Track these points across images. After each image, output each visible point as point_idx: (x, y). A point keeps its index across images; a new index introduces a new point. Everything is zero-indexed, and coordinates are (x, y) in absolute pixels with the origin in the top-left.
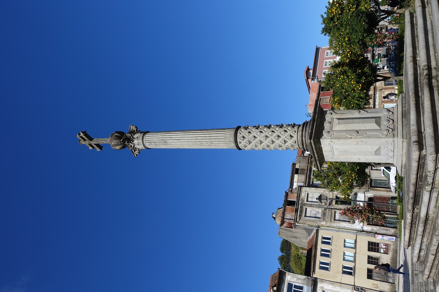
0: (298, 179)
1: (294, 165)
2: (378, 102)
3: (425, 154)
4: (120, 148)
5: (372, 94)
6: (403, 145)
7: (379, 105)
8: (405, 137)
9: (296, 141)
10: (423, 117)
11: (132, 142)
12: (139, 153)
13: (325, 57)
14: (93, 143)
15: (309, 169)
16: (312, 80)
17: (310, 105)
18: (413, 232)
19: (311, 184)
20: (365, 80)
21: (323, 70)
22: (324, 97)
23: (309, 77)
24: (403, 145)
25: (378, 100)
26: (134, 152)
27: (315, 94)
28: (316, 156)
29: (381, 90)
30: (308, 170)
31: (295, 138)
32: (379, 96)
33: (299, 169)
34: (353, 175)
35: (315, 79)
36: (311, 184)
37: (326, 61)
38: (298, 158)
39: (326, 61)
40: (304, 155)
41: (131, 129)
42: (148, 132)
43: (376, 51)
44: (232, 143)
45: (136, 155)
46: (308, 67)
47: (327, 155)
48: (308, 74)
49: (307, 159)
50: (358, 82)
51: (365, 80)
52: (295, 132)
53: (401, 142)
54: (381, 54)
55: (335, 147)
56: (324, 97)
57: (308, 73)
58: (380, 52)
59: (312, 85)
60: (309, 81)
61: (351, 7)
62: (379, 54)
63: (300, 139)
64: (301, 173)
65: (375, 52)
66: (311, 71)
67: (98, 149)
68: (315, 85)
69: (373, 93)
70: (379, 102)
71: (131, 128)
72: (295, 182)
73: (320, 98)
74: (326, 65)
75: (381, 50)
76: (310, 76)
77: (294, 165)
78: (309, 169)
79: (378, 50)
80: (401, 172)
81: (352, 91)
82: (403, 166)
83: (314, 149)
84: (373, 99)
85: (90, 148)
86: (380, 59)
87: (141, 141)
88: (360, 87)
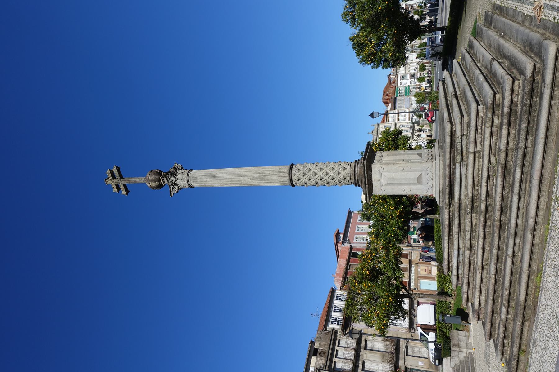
0: (316, 362)
1: (312, 343)
2: (414, 276)
3: (455, 129)
4: (156, 186)
5: (408, 268)
6: (440, 164)
7: (415, 280)
8: (442, 156)
9: (349, 173)
10: (453, 116)
11: (175, 175)
12: (177, 192)
13: (356, 231)
14: (121, 183)
15: (331, 347)
16: (342, 244)
17: (338, 275)
18: (451, 246)
19: (333, 368)
20: (402, 208)
21: (355, 235)
22: (355, 264)
23: (338, 241)
24: (440, 164)
25: (414, 274)
26: (172, 190)
27: (344, 261)
28: (367, 183)
29: (417, 264)
30: (331, 349)
31: (348, 170)
32: (415, 270)
33: (318, 349)
34: (390, 298)
35: (345, 243)
36: (333, 368)
37: (359, 226)
38: (319, 332)
39: (359, 226)
40: (326, 329)
41: (176, 167)
42: (192, 170)
43: (411, 224)
44: (286, 176)
45: (173, 193)
46: (339, 230)
47: (376, 186)
48: (337, 239)
49: (330, 334)
50: (396, 209)
51: (402, 208)
52: (348, 165)
53: (439, 160)
54: (416, 228)
55: (383, 175)
56: (355, 264)
57: (338, 237)
58: (415, 225)
59: (341, 250)
60: (338, 246)
61: (389, 148)
62: (414, 228)
63: (352, 170)
64: (320, 356)
65: (410, 224)
66: (341, 236)
67: (124, 192)
68: (346, 250)
69: (408, 266)
70: (415, 277)
71: (176, 166)
72: (312, 367)
73: (350, 264)
74: (358, 230)
75: (416, 224)
76: (340, 240)
77: (312, 343)
78: (331, 347)
79: (414, 223)
80: (439, 200)
81: (391, 216)
82: (441, 191)
83: (366, 173)
84: (408, 272)
85: (115, 190)
86: (415, 232)
87: (185, 176)
88: (398, 213)
